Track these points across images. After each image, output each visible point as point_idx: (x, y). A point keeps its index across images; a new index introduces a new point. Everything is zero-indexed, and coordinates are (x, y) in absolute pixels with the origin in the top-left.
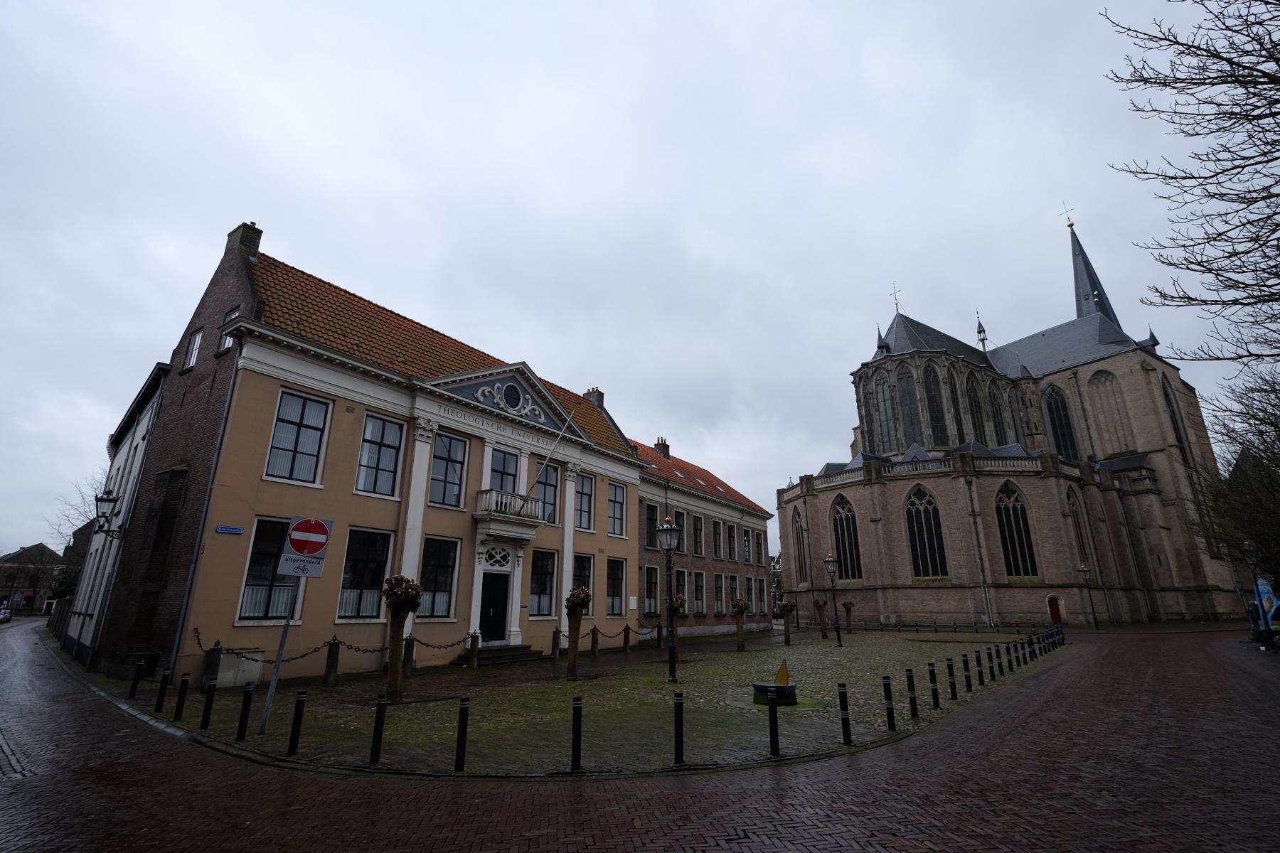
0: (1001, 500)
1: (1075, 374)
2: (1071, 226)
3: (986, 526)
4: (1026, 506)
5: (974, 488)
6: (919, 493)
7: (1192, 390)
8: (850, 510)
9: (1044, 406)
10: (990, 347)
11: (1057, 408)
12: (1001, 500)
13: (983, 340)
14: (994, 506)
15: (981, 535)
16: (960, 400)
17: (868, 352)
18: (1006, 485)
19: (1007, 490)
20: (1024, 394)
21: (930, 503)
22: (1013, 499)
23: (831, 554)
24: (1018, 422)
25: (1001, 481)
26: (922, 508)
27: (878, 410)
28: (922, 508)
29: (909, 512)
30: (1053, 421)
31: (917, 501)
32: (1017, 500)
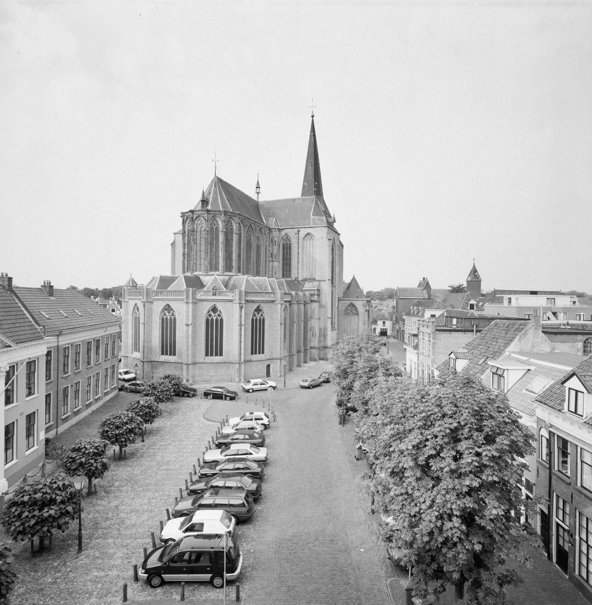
0: (255, 315)
1: (299, 232)
2: (313, 116)
3: (245, 330)
4: (265, 318)
5: (243, 310)
6: (214, 309)
7: (343, 246)
8: (173, 315)
9: (281, 246)
10: (262, 199)
11: (287, 248)
12: (255, 315)
13: (258, 193)
14: (251, 318)
15: (243, 336)
16: (242, 244)
17: (193, 203)
18: (258, 307)
19: (258, 310)
20: (274, 237)
21: (219, 315)
22: (260, 314)
23: (202, 503)
24: (268, 251)
25: (255, 306)
26: (214, 318)
27: (195, 243)
28: (214, 318)
29: (207, 320)
30: (283, 255)
31: (213, 314)
32: (262, 315)
